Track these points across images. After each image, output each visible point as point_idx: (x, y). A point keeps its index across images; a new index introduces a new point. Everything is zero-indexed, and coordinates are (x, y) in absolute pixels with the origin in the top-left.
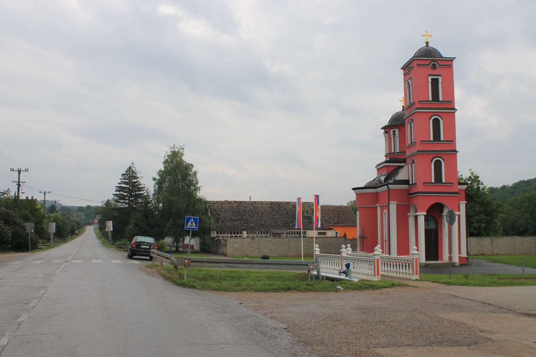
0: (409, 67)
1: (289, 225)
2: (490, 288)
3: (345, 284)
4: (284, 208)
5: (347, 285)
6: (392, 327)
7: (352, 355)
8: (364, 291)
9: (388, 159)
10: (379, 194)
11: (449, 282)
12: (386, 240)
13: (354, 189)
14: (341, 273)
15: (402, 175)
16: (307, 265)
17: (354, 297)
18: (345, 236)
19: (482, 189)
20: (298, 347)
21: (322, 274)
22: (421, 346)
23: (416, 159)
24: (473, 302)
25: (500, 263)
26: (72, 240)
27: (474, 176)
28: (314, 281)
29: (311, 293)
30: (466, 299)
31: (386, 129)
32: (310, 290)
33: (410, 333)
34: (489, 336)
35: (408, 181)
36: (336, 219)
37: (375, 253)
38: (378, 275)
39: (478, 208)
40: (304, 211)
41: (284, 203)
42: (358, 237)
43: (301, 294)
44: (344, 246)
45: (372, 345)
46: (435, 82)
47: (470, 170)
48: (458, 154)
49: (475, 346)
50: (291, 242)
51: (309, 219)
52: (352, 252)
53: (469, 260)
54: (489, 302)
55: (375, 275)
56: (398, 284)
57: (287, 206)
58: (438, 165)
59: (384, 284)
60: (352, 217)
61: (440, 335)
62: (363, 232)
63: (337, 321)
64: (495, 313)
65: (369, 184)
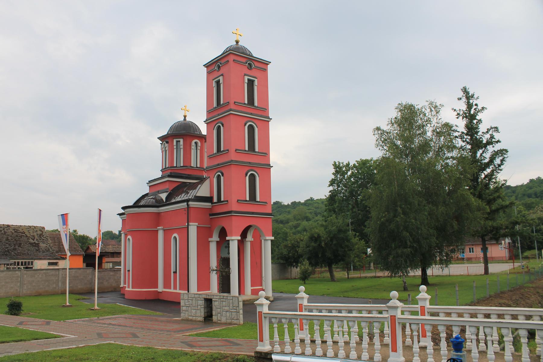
1: (11, 253)
4: (3, 232)
12: (129, 271)
36: (56, 247)
40: (30, 237)
41: (3, 226)
42: (68, 268)
46: (251, 83)
50: (25, 276)
51: (35, 246)
57: (7, 230)
60: (74, 245)
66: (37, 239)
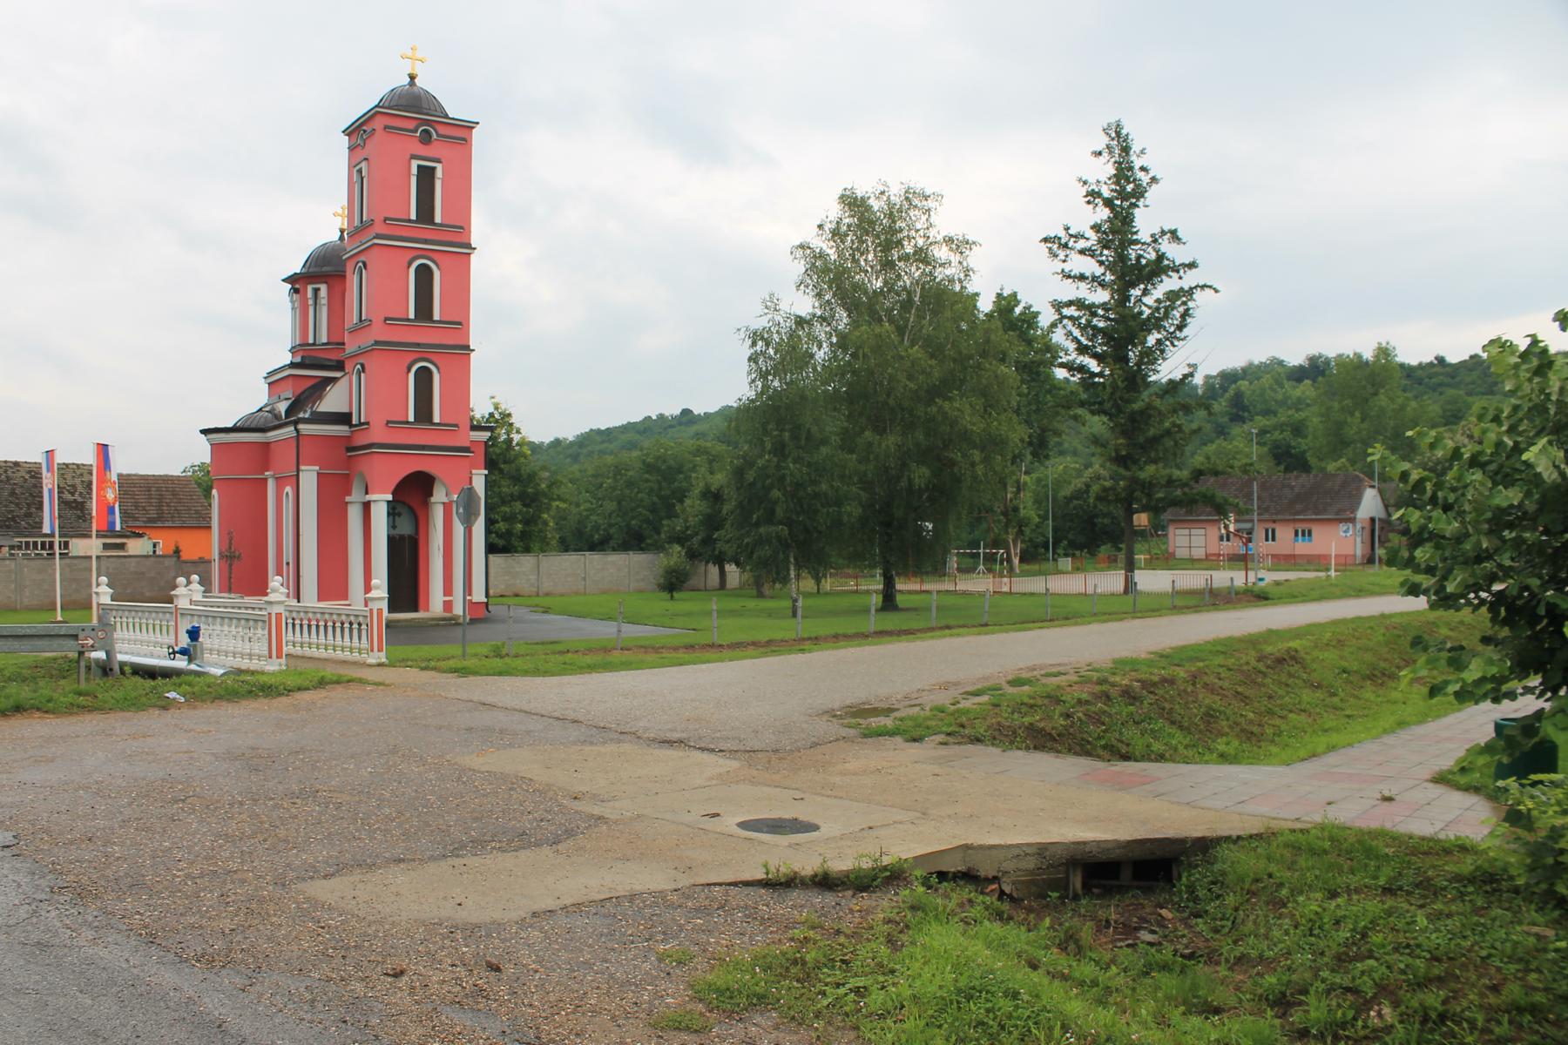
0: (365, 131)
2: (565, 679)
3: (189, 685)
5: (196, 689)
6: (339, 806)
7: (237, 916)
8: (245, 703)
9: (298, 359)
10: (272, 446)
11: (464, 668)
12: (288, 564)
13: (205, 432)
14: (174, 653)
15: (333, 401)
16: (75, 637)
17: (218, 722)
18: (177, 552)
19: (517, 444)
20: (53, 914)
21: (120, 657)
22: (433, 858)
23: (372, 363)
24: (535, 717)
25: (560, 614)
26: (1109, 568)
27: (500, 414)
28: (97, 683)
29: (88, 717)
30: (516, 710)
31: (297, 282)
32: (84, 707)
33: (393, 821)
34: (597, 811)
35: (350, 415)
37: (272, 597)
38: (279, 656)
39: (507, 488)
43: (58, 721)
44: (181, 580)
45: (292, 874)
46: (426, 176)
47: (493, 398)
48: (473, 355)
49: (570, 842)
51: (76, 508)
52: (204, 597)
53: (490, 608)
54: (571, 715)
55: (270, 657)
56: (335, 679)
58: (424, 378)
59: (299, 681)
61: (476, 819)
62: (230, 543)
63: (177, 801)
64: (592, 743)
65: (246, 421)
66: (81, 494)
